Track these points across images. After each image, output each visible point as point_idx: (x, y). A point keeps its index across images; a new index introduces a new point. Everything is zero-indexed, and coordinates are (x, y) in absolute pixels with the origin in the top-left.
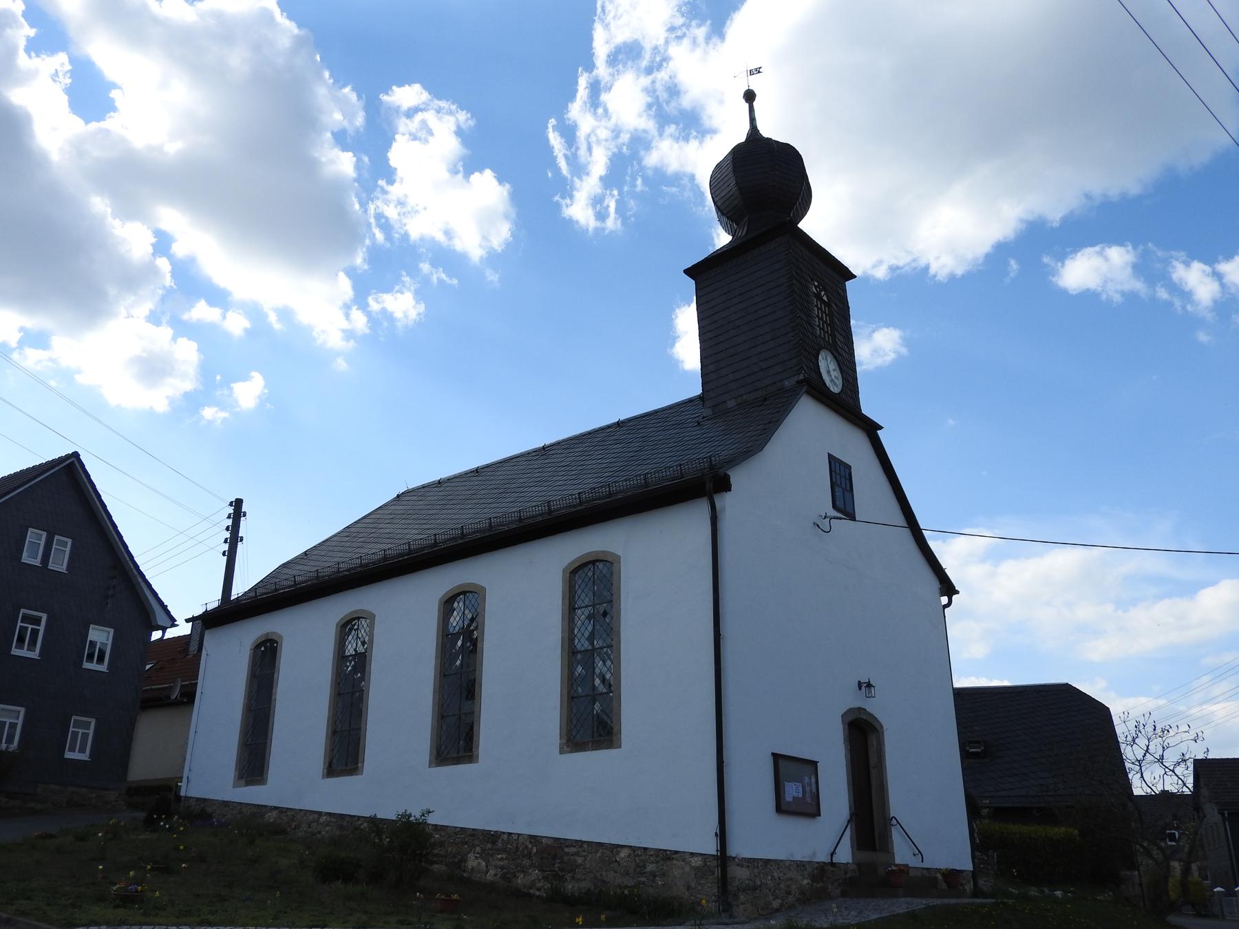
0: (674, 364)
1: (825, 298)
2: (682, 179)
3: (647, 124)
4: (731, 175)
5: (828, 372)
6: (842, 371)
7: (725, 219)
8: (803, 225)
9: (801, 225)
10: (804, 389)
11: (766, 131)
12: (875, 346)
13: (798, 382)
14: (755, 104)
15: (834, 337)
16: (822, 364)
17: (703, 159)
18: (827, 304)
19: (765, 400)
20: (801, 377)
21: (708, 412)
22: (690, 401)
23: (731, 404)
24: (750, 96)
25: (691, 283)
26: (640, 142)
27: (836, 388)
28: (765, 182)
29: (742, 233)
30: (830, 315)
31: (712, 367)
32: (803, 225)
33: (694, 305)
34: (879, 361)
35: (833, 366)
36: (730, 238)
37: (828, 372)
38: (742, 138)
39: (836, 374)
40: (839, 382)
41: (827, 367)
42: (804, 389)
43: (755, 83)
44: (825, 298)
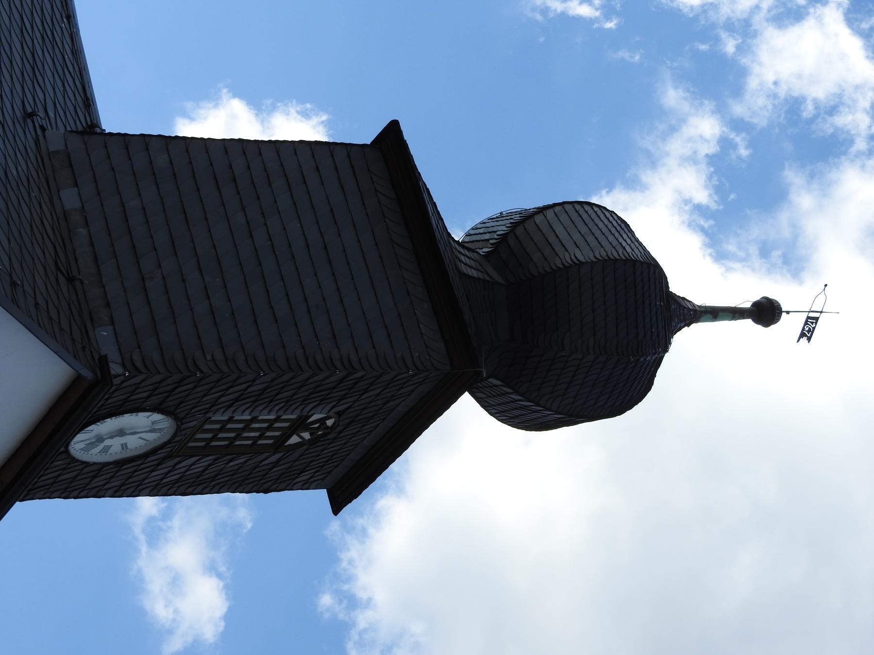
0: (205, 94)
1: (294, 440)
2: (626, 172)
3: (754, 105)
4: (600, 253)
5: (121, 433)
6: (119, 464)
7: (502, 229)
8: (466, 405)
9: (466, 401)
10: (86, 373)
11: (686, 342)
12: (184, 553)
13: (103, 362)
14: (748, 323)
15: (205, 450)
16: (141, 420)
17: (662, 222)
18: (279, 444)
19: (71, 280)
20: (115, 369)
21: (55, 140)
22: (88, 102)
23: (70, 198)
24: (766, 312)
25: (365, 135)
26: (717, 77)
27: (84, 445)
28: (575, 328)
29: (468, 267)
30: (254, 448)
31: (161, 160)
32: (466, 405)
33: (324, 139)
34: (156, 584)
35: (135, 444)
36: (458, 235)
37: (121, 433)
38: (677, 287)
39: (115, 449)
40: (94, 456)
41: (137, 430)
42: (86, 373)
43: (789, 325)
44: (294, 440)
